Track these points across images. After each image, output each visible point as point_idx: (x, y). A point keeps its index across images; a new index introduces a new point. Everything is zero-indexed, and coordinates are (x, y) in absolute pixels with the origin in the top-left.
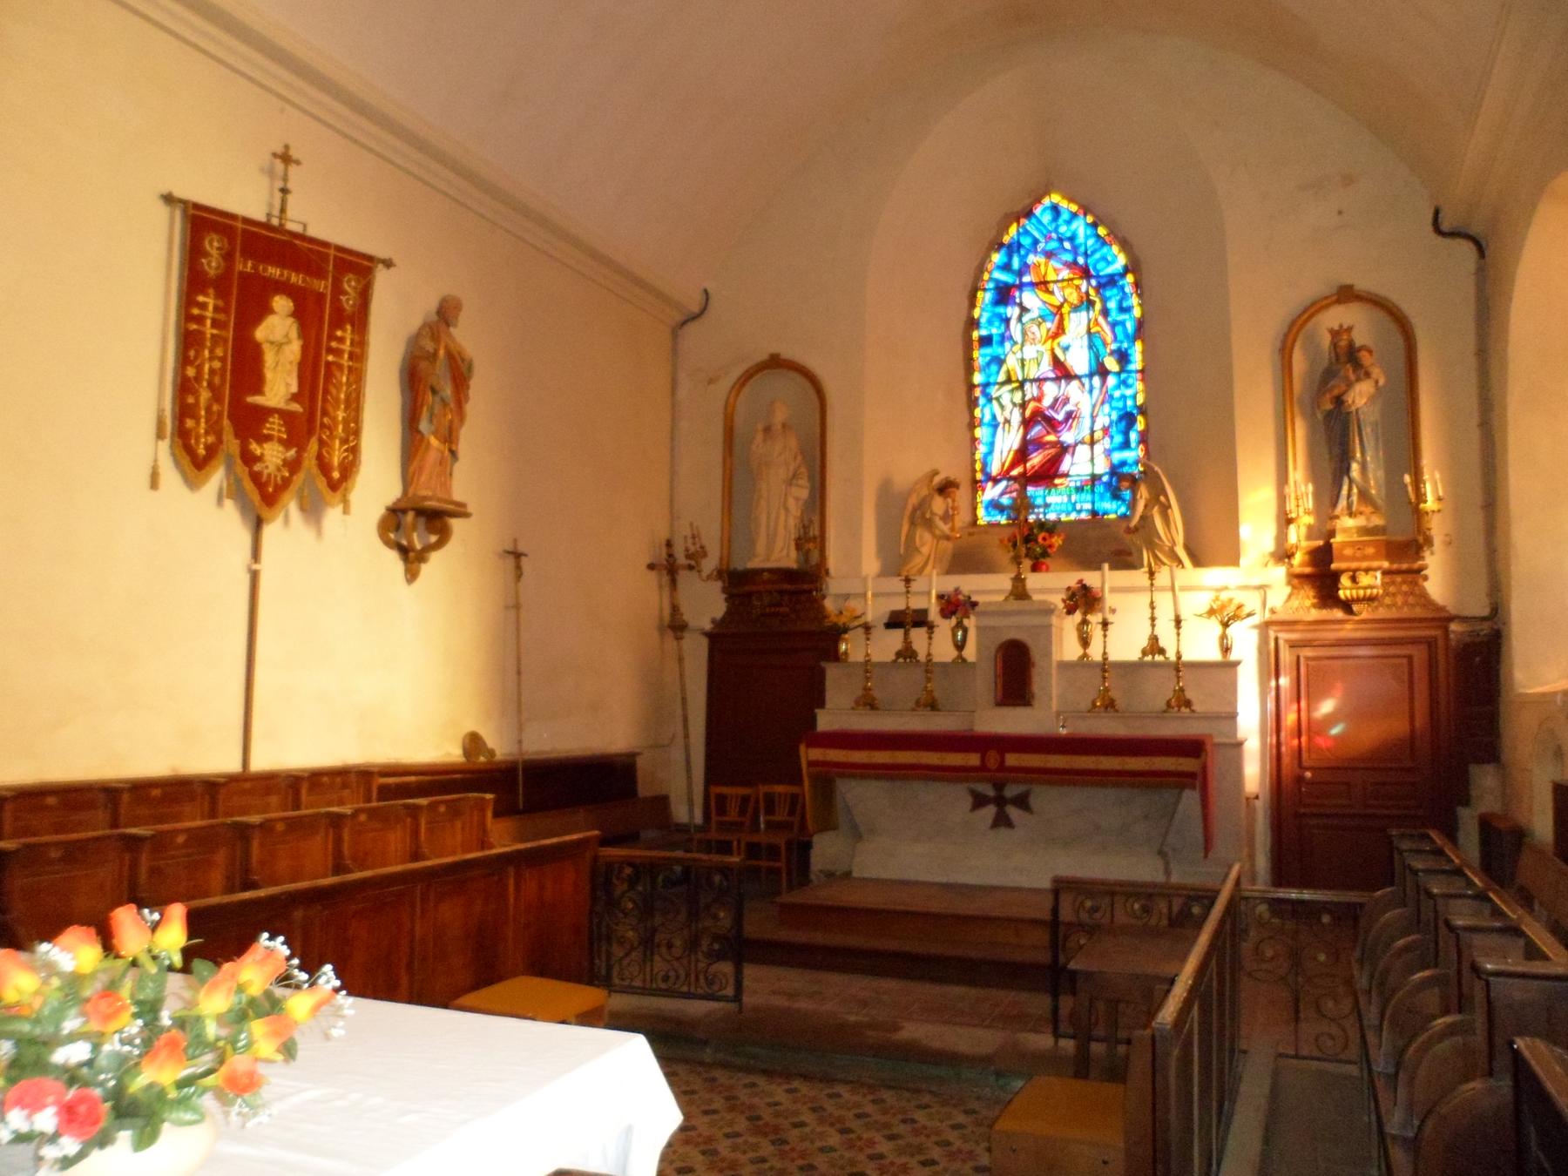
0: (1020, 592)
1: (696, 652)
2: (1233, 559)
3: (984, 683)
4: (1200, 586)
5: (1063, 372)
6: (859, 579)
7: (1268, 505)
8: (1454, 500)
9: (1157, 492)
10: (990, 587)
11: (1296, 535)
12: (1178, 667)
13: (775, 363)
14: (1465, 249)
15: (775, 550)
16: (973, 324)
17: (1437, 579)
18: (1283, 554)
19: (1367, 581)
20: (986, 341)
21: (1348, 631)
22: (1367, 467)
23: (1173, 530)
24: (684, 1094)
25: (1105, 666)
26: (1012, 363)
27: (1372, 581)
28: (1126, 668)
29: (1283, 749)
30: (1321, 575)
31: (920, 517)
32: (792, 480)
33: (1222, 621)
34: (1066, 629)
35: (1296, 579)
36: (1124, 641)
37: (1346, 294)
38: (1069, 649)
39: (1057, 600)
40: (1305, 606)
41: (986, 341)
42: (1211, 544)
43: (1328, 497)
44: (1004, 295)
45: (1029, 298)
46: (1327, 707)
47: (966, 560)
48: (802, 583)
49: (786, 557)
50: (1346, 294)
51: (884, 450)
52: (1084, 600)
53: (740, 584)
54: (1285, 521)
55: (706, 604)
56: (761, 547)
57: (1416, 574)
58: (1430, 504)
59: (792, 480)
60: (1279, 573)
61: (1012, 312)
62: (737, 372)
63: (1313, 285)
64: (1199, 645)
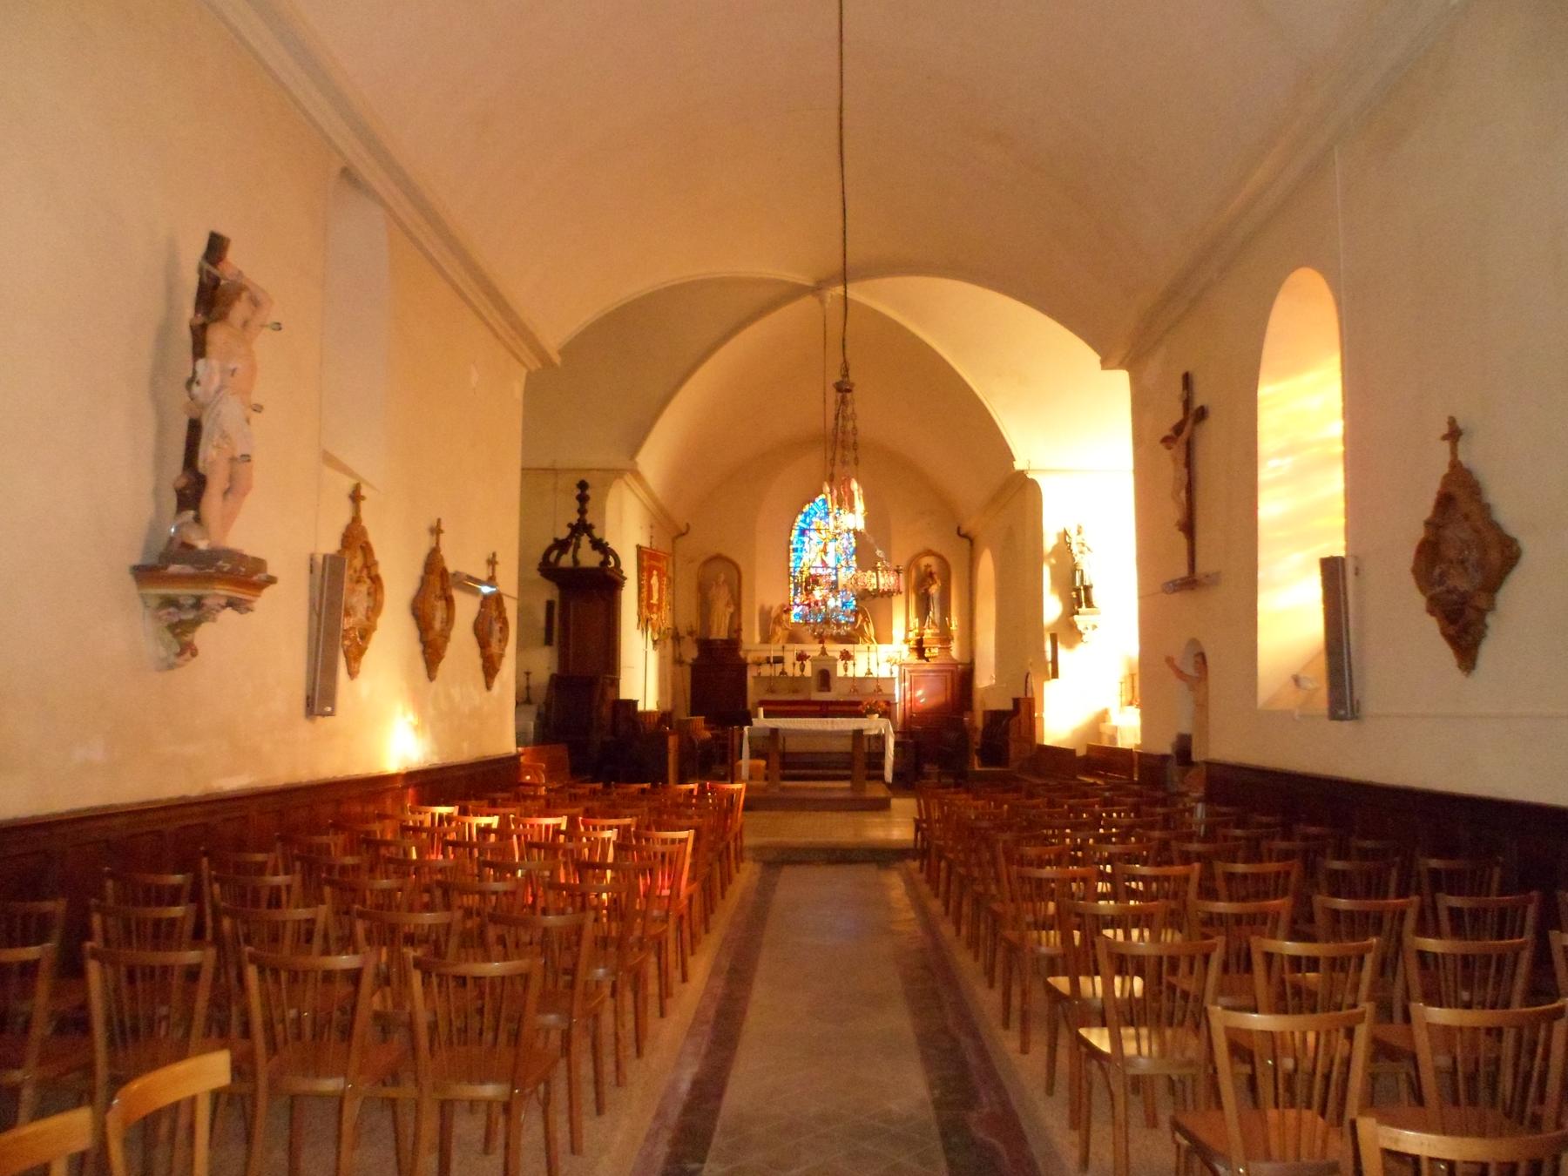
0: (824, 652)
1: (687, 671)
2: (890, 640)
3: (814, 684)
4: (884, 651)
5: (825, 565)
6: (752, 643)
7: (902, 620)
8: (961, 627)
9: (865, 616)
10: (813, 649)
11: (912, 635)
12: (877, 679)
13: (718, 558)
14: (966, 543)
15: (720, 632)
16: (790, 543)
17: (955, 651)
18: (907, 641)
19: (933, 651)
20: (795, 550)
21: (927, 667)
22: (935, 613)
23: (870, 630)
24: (233, 1080)
25: (854, 678)
26: (805, 560)
27: (935, 651)
28: (861, 679)
29: (1177, 663)
30: (920, 649)
31: (778, 621)
32: (728, 605)
33: (887, 660)
34: (840, 664)
35: (912, 649)
36: (858, 669)
37: (929, 553)
38: (840, 672)
39: (837, 655)
40: (913, 658)
41: (795, 550)
42: (883, 637)
43: (922, 623)
44: (803, 532)
45: (813, 534)
46: (919, 693)
47: (793, 638)
48: (733, 644)
49: (723, 635)
50: (929, 553)
51: (764, 593)
52: (846, 656)
53: (706, 646)
54: (908, 630)
55: (691, 653)
56: (715, 629)
57: (948, 649)
58: (953, 628)
59: (728, 605)
60: (906, 647)
61: (806, 539)
62: (703, 559)
63: (919, 548)
64: (882, 672)
